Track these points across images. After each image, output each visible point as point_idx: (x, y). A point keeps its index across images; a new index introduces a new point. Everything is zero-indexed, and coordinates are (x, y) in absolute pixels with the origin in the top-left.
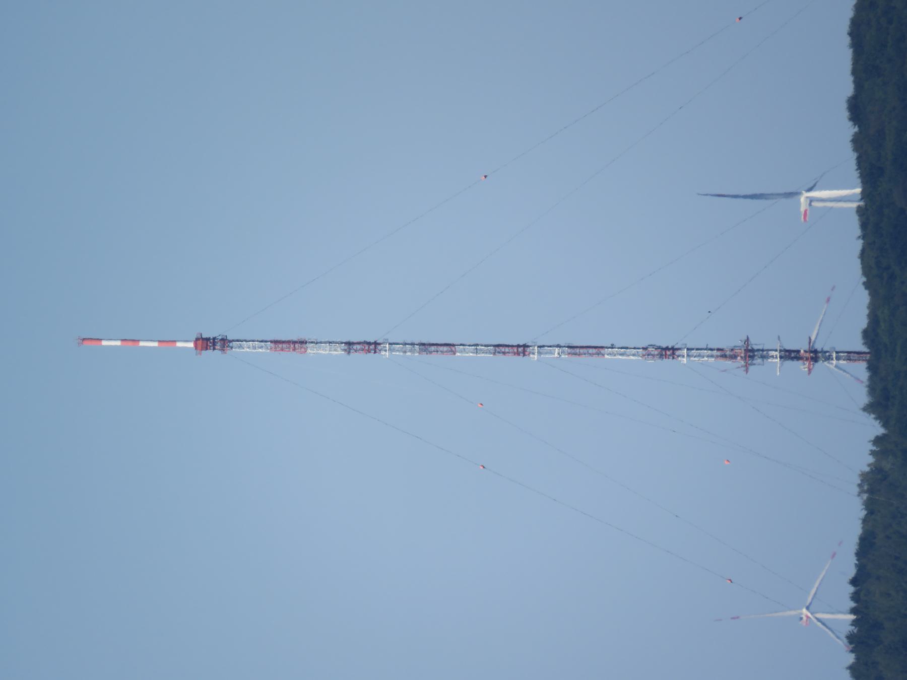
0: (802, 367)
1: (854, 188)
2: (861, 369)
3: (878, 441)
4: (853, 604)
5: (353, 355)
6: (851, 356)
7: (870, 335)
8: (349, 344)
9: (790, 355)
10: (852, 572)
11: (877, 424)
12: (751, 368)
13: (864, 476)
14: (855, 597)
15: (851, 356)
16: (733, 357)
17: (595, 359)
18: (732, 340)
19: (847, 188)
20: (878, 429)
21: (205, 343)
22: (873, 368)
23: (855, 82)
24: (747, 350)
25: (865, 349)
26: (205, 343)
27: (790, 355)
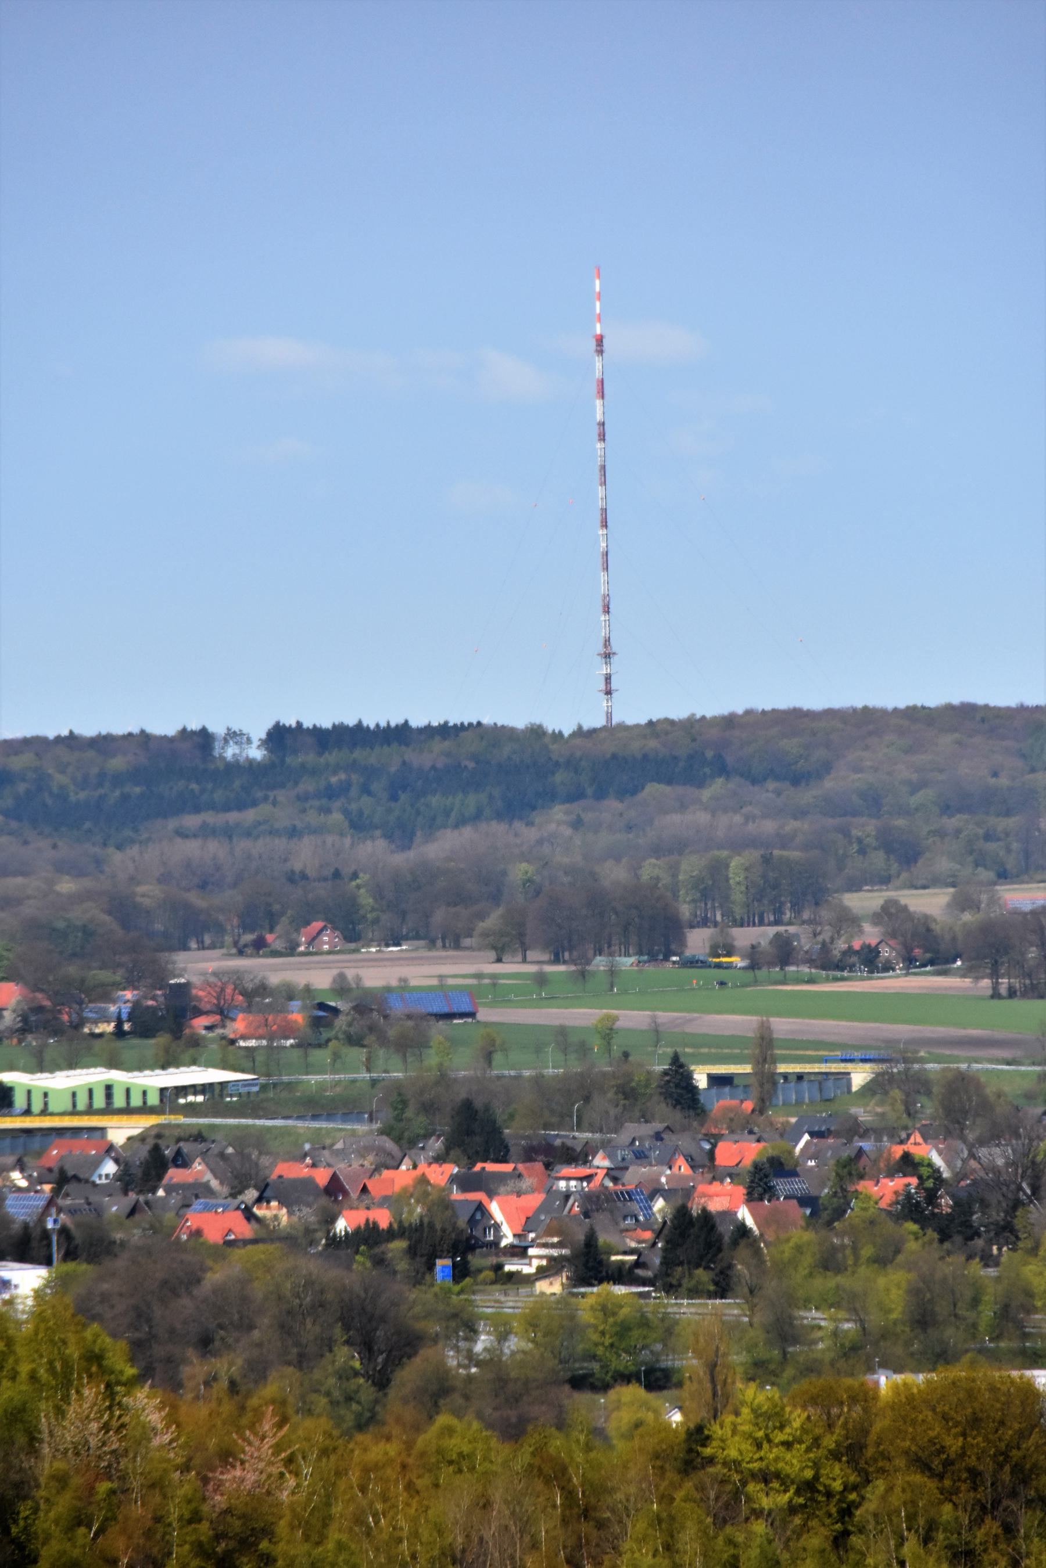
0: (603, 687)
1: (595, 406)
2: (599, 722)
3: (560, 732)
4: (466, 724)
5: (597, 427)
6: (609, 716)
7: (622, 727)
8: (603, 424)
9: (608, 678)
10: (766, 709)
11: (570, 731)
12: (599, 658)
13: (540, 727)
14: (470, 725)
15: (609, 716)
16: (606, 646)
17: (600, 567)
18: (615, 646)
19: (781, 990)
20: (566, 733)
21: (600, 340)
22: (604, 728)
23: (1008, 709)
24: (609, 654)
25: (614, 723)
26: (600, 340)
27: (608, 678)
